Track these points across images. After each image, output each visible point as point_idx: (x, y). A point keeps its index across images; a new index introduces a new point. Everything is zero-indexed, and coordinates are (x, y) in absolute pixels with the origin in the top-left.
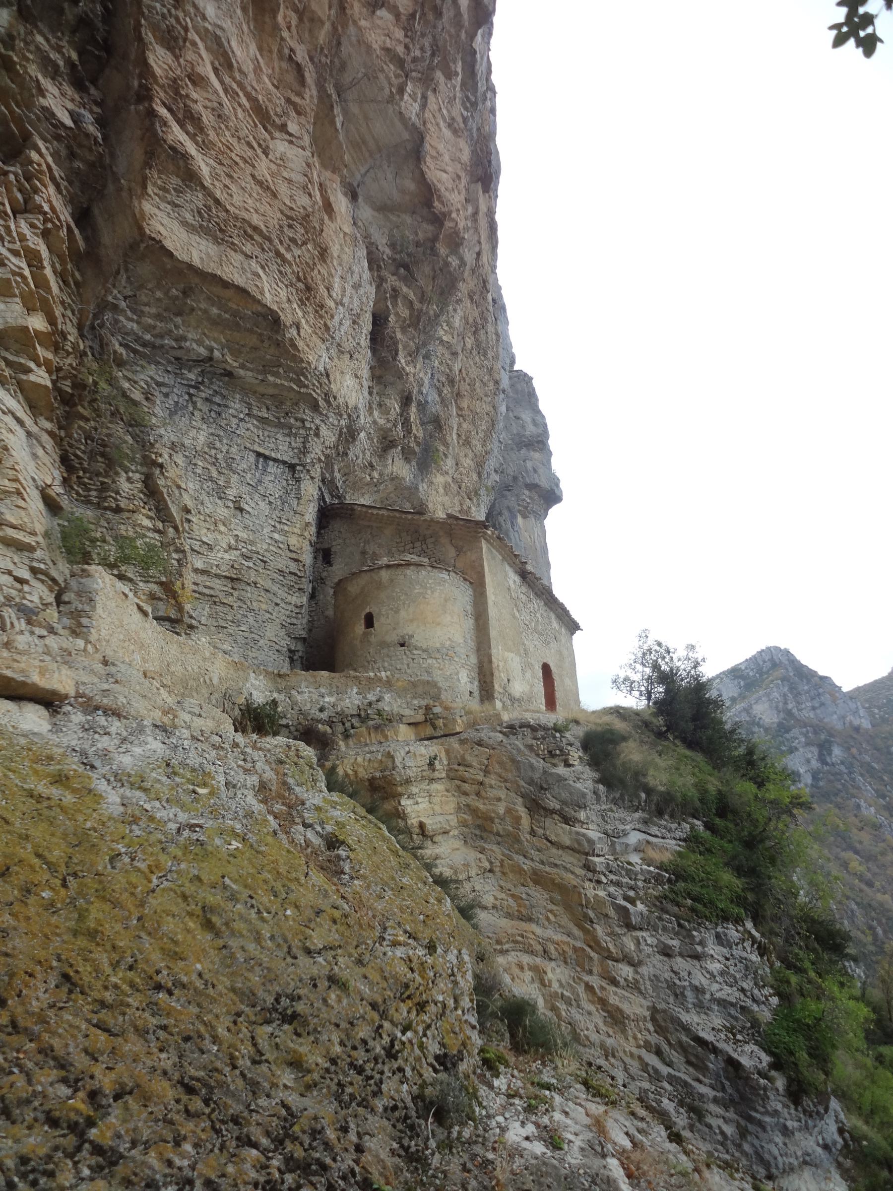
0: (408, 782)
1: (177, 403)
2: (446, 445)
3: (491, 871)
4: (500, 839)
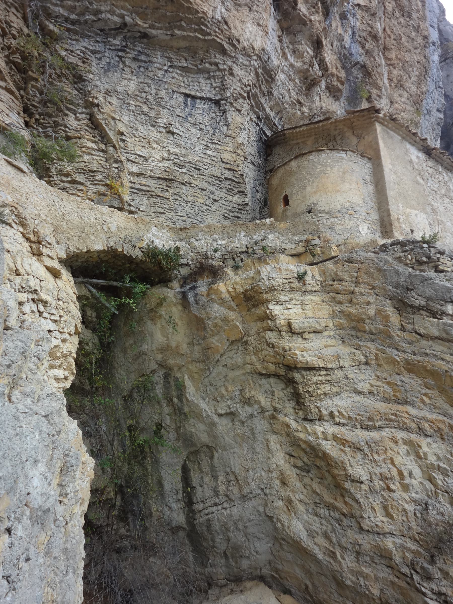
0: (272, 289)
1: (109, 63)
2: (379, 89)
3: (367, 364)
4: (373, 337)
